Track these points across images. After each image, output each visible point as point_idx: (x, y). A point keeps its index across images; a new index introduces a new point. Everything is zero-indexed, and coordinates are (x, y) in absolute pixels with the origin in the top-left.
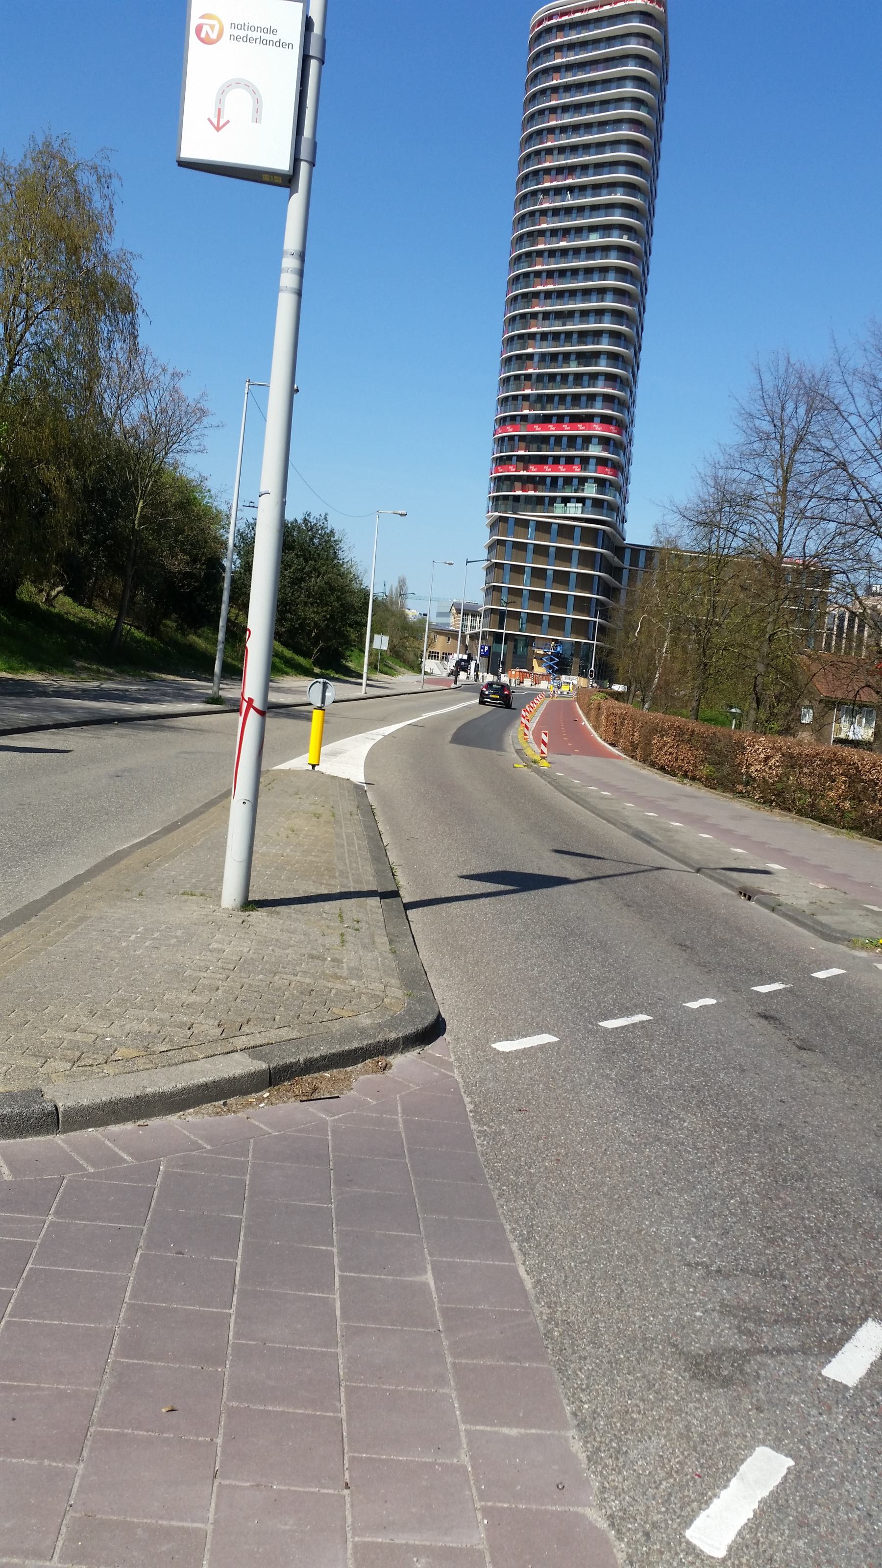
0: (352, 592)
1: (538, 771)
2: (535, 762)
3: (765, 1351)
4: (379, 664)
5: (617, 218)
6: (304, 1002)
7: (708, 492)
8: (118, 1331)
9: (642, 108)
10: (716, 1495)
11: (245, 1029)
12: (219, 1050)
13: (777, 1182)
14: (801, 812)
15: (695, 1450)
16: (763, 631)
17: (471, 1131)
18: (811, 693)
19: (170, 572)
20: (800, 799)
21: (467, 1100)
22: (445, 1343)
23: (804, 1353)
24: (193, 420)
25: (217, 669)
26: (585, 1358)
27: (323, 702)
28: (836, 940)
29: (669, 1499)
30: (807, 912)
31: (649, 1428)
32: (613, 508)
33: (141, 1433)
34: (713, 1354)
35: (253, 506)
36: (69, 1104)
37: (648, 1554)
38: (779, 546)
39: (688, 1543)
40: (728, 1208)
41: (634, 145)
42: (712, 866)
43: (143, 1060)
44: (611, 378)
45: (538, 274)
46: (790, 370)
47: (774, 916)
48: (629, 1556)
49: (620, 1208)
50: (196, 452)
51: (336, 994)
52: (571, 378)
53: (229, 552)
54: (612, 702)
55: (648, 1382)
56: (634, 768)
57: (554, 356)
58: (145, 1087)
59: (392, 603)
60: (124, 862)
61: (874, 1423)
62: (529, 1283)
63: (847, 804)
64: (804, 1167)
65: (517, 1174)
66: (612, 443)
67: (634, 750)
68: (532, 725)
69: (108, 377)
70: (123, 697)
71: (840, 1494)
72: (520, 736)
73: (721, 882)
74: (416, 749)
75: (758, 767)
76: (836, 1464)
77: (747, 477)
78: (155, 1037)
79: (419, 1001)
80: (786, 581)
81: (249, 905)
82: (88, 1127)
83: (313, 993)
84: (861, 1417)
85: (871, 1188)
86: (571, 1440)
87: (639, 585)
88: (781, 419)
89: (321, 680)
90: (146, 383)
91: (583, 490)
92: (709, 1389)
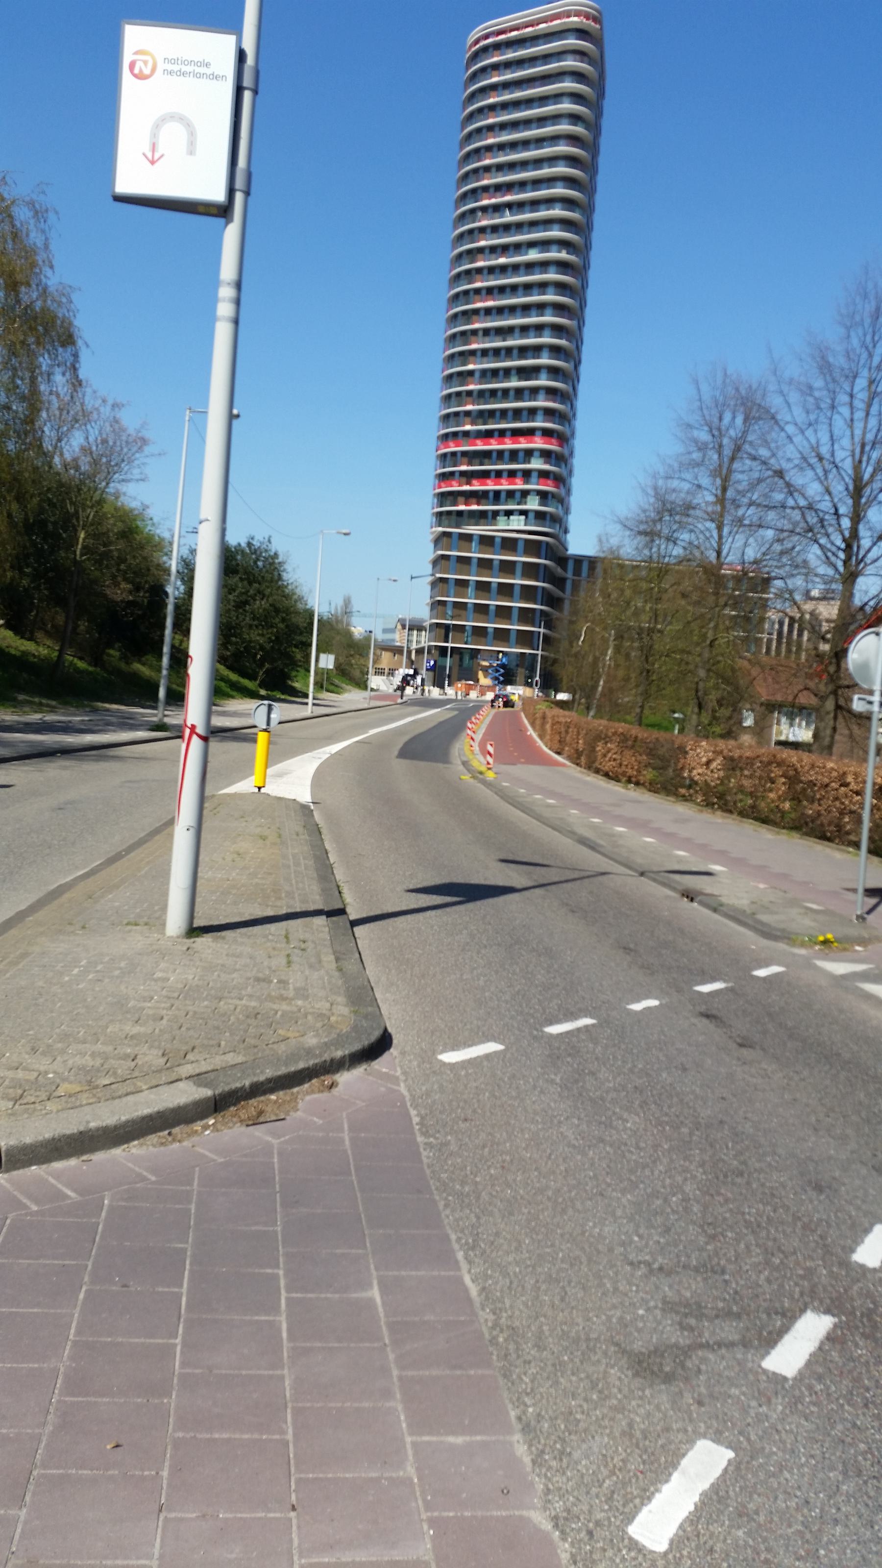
0: (297, 613)
1: (484, 782)
2: (481, 773)
3: (707, 1346)
4: (325, 683)
5: (556, 233)
6: (249, 1025)
7: (648, 502)
8: (62, 1370)
9: (580, 123)
10: (658, 1490)
11: (190, 1057)
12: (164, 1079)
13: (717, 1178)
14: (743, 814)
15: (637, 1446)
16: (704, 637)
17: (417, 1145)
18: (752, 697)
19: (113, 601)
20: (741, 801)
21: (413, 1112)
22: (391, 1357)
23: (745, 1346)
24: (135, 449)
25: (162, 693)
26: (530, 1362)
27: (268, 723)
28: (775, 938)
29: (612, 1496)
30: (749, 911)
31: (592, 1428)
32: (555, 520)
33: (85, 1472)
34: (656, 1351)
35: (195, 532)
36: (12, 1143)
37: (591, 1552)
38: (719, 553)
39: (631, 1539)
40: (670, 1205)
41: (572, 160)
42: (655, 869)
43: (86, 1095)
44: (551, 392)
45: (477, 291)
46: (728, 381)
47: (716, 916)
48: (573, 1555)
49: (564, 1211)
50: (137, 480)
51: (282, 1016)
52: (512, 393)
53: (173, 578)
54: (557, 711)
55: (592, 1382)
56: (579, 775)
57: (495, 373)
58: (88, 1122)
59: (337, 621)
60: (67, 896)
61: (812, 1412)
62: (474, 1291)
63: (787, 805)
64: (744, 1163)
65: (463, 1183)
66: (553, 456)
67: (579, 758)
68: (478, 737)
69: (48, 410)
70: (66, 729)
71: (779, 1483)
72: (467, 748)
73: (664, 884)
74: (363, 766)
75: (700, 771)
76: (775, 1454)
77: (686, 486)
78: (98, 1070)
79: (366, 1017)
80: (726, 588)
81: (194, 931)
82: (31, 1165)
83: (259, 1016)
84: (800, 1406)
85: (810, 1182)
86: (516, 1445)
87: (582, 594)
88: (719, 429)
89: (266, 702)
90: (86, 415)
91: (525, 503)
92: (651, 1386)
